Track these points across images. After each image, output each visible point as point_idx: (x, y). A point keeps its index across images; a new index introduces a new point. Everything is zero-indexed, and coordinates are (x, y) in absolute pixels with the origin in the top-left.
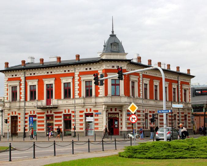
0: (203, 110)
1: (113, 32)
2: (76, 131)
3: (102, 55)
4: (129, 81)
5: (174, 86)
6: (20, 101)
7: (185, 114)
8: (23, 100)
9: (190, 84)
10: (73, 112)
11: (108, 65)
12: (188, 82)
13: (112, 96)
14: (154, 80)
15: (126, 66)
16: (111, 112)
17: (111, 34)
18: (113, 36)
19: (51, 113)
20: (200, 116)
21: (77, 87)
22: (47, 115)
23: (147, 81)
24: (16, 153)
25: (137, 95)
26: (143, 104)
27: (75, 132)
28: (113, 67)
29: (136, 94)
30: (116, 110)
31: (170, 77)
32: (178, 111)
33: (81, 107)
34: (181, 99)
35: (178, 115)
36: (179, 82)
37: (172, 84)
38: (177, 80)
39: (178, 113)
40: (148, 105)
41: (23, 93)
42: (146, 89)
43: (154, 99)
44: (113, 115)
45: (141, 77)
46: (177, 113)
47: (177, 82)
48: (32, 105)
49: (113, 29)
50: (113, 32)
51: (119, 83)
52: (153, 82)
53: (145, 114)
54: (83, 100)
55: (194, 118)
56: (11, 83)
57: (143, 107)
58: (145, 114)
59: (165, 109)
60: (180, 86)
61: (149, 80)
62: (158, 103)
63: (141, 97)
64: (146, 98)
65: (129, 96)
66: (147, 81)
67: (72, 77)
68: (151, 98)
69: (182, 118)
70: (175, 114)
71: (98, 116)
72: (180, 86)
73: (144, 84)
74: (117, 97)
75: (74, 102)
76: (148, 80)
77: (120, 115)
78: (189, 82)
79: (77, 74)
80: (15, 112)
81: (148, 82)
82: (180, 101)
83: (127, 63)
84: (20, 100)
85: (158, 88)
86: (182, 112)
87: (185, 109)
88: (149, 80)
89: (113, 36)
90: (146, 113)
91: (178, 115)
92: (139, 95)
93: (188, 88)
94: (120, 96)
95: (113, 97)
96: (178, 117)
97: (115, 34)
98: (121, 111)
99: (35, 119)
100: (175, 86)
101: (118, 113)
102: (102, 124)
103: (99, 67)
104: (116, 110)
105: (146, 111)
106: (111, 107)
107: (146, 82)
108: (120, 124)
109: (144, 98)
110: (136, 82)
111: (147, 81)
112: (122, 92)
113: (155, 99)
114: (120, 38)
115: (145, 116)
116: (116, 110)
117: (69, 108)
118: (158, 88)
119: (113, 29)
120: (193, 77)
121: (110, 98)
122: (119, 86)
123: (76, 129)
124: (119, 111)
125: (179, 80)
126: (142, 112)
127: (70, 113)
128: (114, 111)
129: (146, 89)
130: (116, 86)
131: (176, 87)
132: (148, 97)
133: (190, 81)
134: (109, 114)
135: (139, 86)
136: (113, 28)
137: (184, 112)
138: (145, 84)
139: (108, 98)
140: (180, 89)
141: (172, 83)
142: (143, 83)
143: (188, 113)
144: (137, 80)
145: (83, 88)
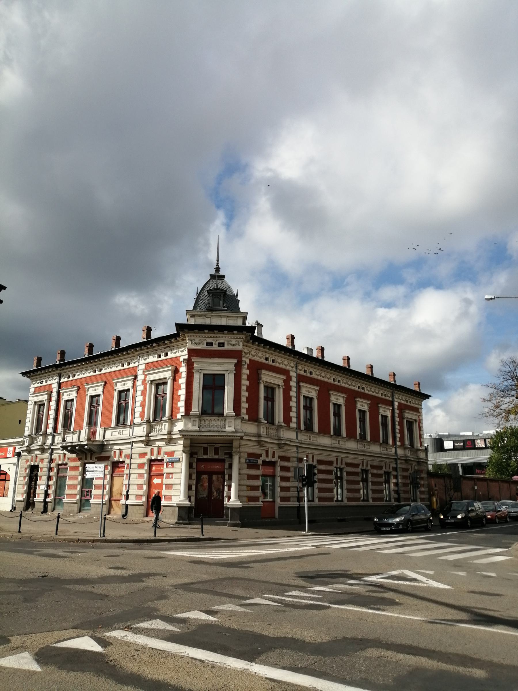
1: (218, 269)
3: (191, 314)
5: (385, 411)
7: (384, 469)
8: (50, 431)
9: (420, 410)
11: (197, 340)
12: (415, 406)
14: (331, 392)
15: (241, 344)
16: (205, 457)
17: (213, 272)
20: (488, 481)
21: (139, 398)
23: (310, 391)
25: (282, 420)
26: (297, 441)
28: (209, 344)
29: (279, 417)
30: (216, 452)
31: (417, 403)
32: (395, 466)
33: (142, 445)
34: (402, 439)
35: (395, 473)
36: (396, 404)
37: (329, 394)
38: (390, 399)
39: (393, 468)
40: (342, 449)
43: (332, 433)
45: (294, 379)
46: (391, 470)
47: (392, 404)
49: (218, 263)
50: (218, 269)
52: (378, 408)
54: (282, 436)
55: (433, 482)
57: (300, 449)
58: (385, 472)
60: (397, 411)
61: (318, 388)
62: (341, 443)
63: (293, 425)
64: (309, 428)
65: (253, 418)
66: (310, 391)
67: (235, 361)
70: (364, 468)
71: (173, 467)
72: (397, 411)
74: (215, 417)
76: (316, 390)
77: (227, 466)
78: (418, 406)
81: (313, 394)
82: (398, 443)
84: (46, 431)
85: (279, 395)
86: (404, 466)
87: (411, 462)
90: (387, 470)
91: (395, 473)
92: (287, 419)
93: (416, 418)
94: (225, 415)
95: (205, 417)
96: (396, 477)
97: (221, 273)
98: (231, 456)
100: (362, 406)
101: (223, 461)
102: (176, 492)
103: (233, 342)
104: (216, 453)
105: (337, 464)
106: (206, 445)
107: (337, 399)
108: (194, 488)
109: (302, 427)
110: (277, 390)
111: (364, 404)
112: (228, 408)
113: (335, 434)
117: (122, 447)
119: (218, 263)
121: (197, 420)
123: (130, 496)
124: (226, 454)
125: (395, 399)
126: (295, 459)
128: (211, 455)
131: (389, 414)
133: (421, 405)
134: (199, 460)
135: (287, 399)
136: (218, 261)
137: (410, 467)
139: (192, 419)
140: (397, 419)
141: (330, 390)
142: (299, 393)
144: (281, 383)
145: (279, 415)
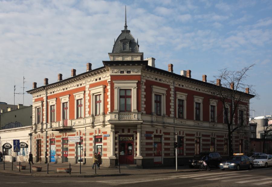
0: (118, 164)
1: (126, 27)
2: (86, 157)
4: (151, 93)
6: (85, 117)
10: (84, 134)
11: (116, 71)
13: (120, 111)
17: (123, 29)
18: (126, 32)
19: (66, 136)
22: (63, 139)
23: (182, 96)
24: (177, 153)
26: (174, 124)
27: (85, 159)
41: (45, 115)
42: (181, 106)
44: (126, 138)
45: (172, 90)
48: (181, 123)
50: (126, 27)
51: (121, 99)
53: (225, 139)
56: (37, 104)
57: (175, 128)
58: (225, 139)
59: (21, 148)
61: (187, 94)
63: (172, 115)
68: (190, 118)
69: (236, 143)
73: (177, 100)
75: (175, 120)
76: (185, 95)
78: (247, 102)
79: (88, 86)
80: (161, 131)
83: (141, 67)
84: (43, 122)
85: (163, 99)
88: (187, 94)
89: (126, 32)
95: (121, 113)
97: (128, 29)
99: (106, 142)
110: (244, 111)
114: (135, 35)
115: (212, 142)
116: (129, 131)
118: (163, 99)
119: (126, 23)
120: (253, 96)
122: (121, 95)
124: (134, 132)
127: (162, 134)
128: (126, 133)
129: (181, 106)
130: (127, 99)
132: (201, 119)
136: (126, 22)
138: (179, 99)
143: (217, 136)
